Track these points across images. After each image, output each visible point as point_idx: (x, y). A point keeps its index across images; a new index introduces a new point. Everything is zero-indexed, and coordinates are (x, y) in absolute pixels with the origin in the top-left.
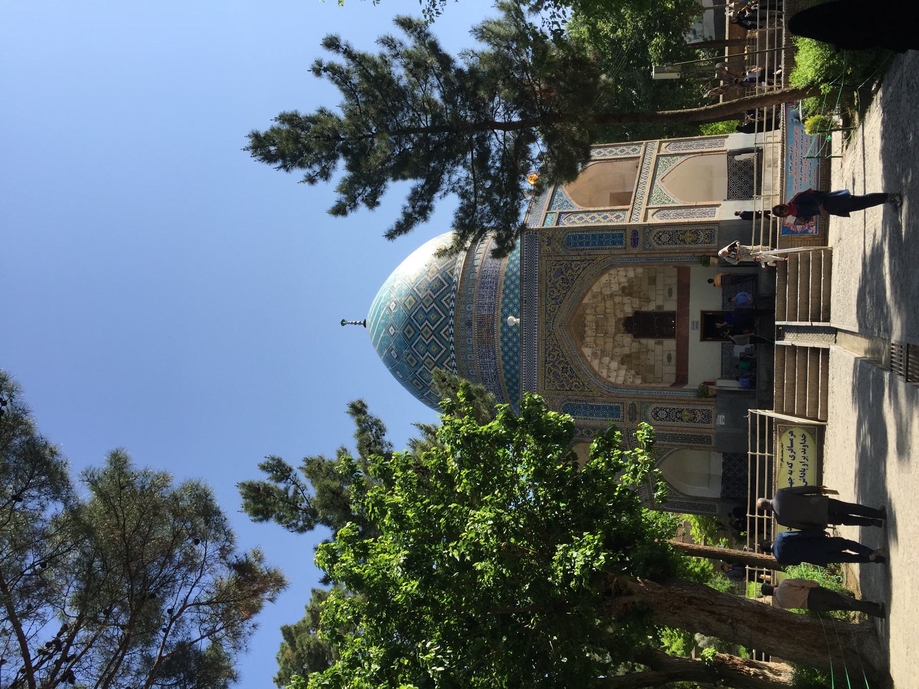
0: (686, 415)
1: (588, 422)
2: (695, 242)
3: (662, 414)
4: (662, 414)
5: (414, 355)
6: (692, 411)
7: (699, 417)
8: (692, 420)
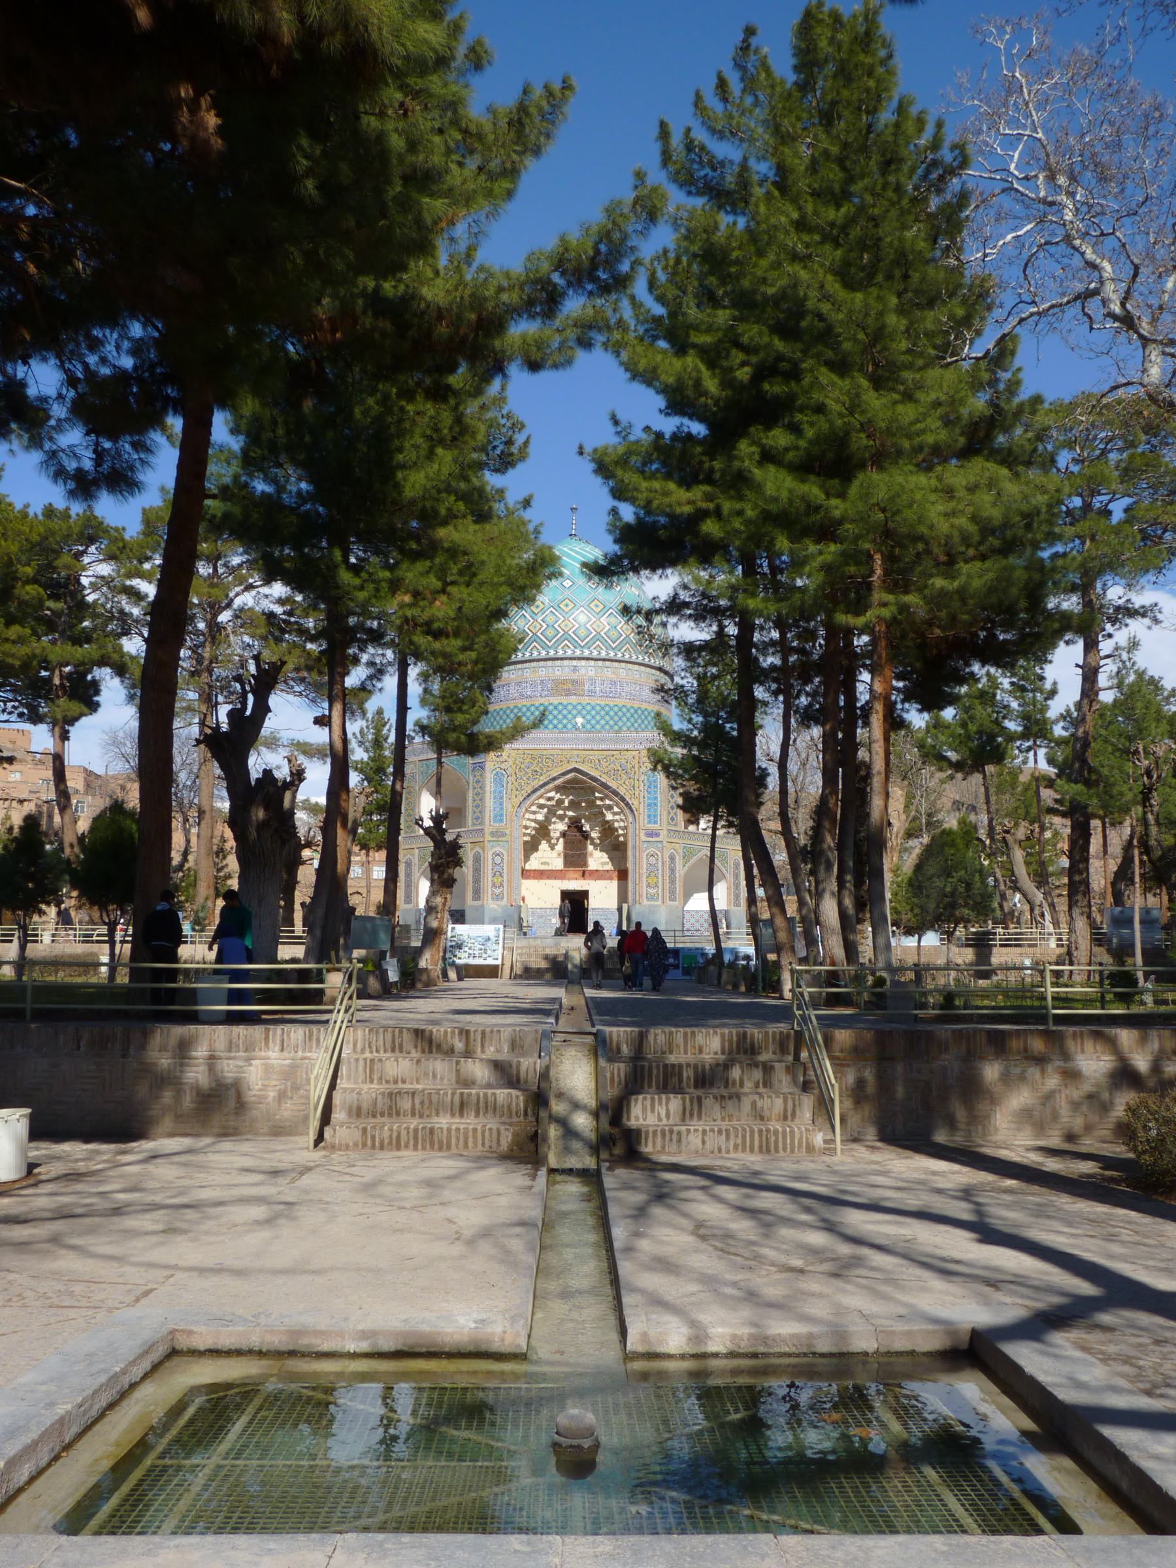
0: (498, 880)
2: (648, 886)
3: (498, 860)
4: (498, 860)
6: (502, 885)
7: (497, 891)
8: (494, 885)
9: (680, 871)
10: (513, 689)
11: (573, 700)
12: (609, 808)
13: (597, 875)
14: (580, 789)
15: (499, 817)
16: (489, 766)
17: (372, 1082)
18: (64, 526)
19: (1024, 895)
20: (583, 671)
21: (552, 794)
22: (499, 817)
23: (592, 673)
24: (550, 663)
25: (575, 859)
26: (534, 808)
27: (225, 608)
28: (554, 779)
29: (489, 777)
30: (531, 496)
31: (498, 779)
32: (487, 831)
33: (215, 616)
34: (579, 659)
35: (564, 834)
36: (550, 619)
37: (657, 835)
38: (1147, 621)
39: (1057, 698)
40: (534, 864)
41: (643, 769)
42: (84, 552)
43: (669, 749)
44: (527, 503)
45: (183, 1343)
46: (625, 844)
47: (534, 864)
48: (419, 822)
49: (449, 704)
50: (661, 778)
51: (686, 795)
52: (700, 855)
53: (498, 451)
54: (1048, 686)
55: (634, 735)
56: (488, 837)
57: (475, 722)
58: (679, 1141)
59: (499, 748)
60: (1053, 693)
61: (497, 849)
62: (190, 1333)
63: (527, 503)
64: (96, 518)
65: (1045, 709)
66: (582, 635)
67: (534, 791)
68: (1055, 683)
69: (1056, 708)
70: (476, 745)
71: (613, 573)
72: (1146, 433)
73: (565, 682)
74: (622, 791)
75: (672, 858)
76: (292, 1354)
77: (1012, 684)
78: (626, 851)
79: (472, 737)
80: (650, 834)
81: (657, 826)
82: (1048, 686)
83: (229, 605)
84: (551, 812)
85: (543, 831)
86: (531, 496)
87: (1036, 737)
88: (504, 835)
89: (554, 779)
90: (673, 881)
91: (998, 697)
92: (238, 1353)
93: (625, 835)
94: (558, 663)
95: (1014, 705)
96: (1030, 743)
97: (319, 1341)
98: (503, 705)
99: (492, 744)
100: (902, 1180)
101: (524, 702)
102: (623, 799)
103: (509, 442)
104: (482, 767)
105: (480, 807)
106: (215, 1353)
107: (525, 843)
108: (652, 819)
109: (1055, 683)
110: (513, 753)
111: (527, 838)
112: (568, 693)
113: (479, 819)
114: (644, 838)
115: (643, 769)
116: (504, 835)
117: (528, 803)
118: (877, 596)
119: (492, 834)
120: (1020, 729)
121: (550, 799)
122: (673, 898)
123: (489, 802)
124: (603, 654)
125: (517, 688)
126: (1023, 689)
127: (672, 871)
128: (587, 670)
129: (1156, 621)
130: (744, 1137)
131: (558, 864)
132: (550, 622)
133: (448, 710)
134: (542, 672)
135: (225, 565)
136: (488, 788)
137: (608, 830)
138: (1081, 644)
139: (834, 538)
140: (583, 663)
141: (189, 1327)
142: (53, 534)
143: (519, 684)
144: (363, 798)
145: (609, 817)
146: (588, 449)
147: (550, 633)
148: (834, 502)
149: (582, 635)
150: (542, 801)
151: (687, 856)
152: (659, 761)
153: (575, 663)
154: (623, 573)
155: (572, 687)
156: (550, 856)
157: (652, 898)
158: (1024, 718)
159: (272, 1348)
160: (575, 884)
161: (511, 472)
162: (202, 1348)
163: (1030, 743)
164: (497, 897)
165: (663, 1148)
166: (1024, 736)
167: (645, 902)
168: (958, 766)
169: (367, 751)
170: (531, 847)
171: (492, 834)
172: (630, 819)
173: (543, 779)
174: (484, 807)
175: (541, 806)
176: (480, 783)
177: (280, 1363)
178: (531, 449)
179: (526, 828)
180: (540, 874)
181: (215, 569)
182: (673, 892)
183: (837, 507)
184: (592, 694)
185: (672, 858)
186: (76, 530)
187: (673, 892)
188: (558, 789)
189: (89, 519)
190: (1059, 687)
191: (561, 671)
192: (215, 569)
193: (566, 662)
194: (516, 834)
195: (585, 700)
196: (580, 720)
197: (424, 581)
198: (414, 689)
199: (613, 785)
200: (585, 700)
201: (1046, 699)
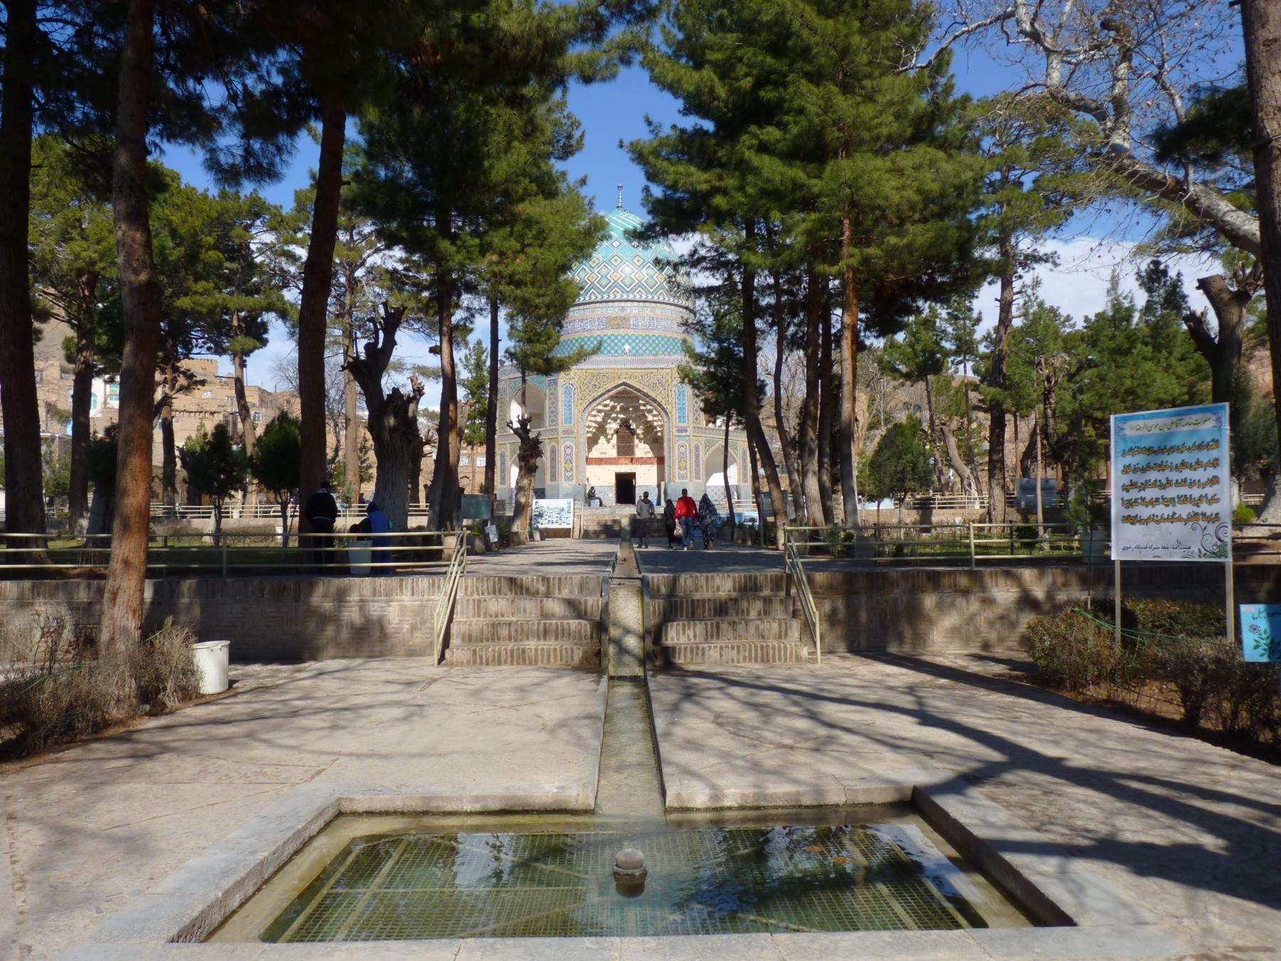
3: (568, 451)
4: (568, 451)
10: (577, 325)
11: (622, 332)
12: (650, 411)
13: (642, 461)
14: (628, 397)
15: (569, 420)
16: (561, 382)
19: (956, 470)
20: (629, 310)
21: (608, 402)
22: (569, 420)
23: (635, 311)
25: (625, 449)
30: (586, 177)
31: (568, 391)
33: (353, 272)
35: (617, 432)
36: (604, 272)
38: (1049, 265)
40: (595, 453)
42: (251, 226)
44: (583, 182)
45: (347, 807)
46: (662, 438)
47: (595, 453)
48: (509, 424)
49: (530, 337)
50: (688, 390)
51: (706, 401)
54: (975, 315)
56: (561, 435)
57: (550, 350)
60: (979, 320)
61: (568, 443)
62: (351, 800)
63: (583, 182)
65: (973, 332)
70: (550, 367)
71: (649, 237)
74: (659, 399)
75: (697, 448)
78: (662, 443)
80: (680, 430)
82: (975, 315)
84: (607, 415)
85: (601, 429)
86: (586, 177)
87: (966, 354)
90: (697, 465)
93: (662, 432)
95: (950, 330)
98: (570, 337)
99: (562, 366)
101: (586, 334)
102: (660, 405)
103: (569, 137)
105: (554, 412)
106: (370, 814)
108: (682, 419)
112: (618, 327)
113: (554, 421)
119: (564, 432)
120: (954, 348)
122: (698, 478)
123: (561, 408)
124: (644, 297)
125: (581, 324)
126: (956, 318)
127: (697, 457)
128: (632, 309)
129: (1056, 265)
131: (613, 453)
134: (599, 311)
135: (359, 233)
137: (649, 428)
142: (228, 212)
143: (581, 320)
144: (468, 407)
145: (650, 418)
146: (626, 143)
150: (600, 407)
151: (708, 445)
152: (686, 376)
155: (620, 322)
156: (607, 448)
157: (683, 477)
160: (625, 468)
164: (569, 479)
166: (957, 353)
167: (678, 481)
168: (907, 376)
170: (593, 441)
171: (564, 432)
173: (601, 391)
175: (600, 411)
176: (554, 395)
178: (586, 141)
180: (600, 461)
182: (698, 473)
184: (636, 327)
185: (697, 448)
186: (245, 208)
187: (698, 473)
188: (612, 398)
191: (613, 310)
194: (581, 432)
195: (631, 332)
196: (627, 347)
198: (503, 327)
200: (631, 332)
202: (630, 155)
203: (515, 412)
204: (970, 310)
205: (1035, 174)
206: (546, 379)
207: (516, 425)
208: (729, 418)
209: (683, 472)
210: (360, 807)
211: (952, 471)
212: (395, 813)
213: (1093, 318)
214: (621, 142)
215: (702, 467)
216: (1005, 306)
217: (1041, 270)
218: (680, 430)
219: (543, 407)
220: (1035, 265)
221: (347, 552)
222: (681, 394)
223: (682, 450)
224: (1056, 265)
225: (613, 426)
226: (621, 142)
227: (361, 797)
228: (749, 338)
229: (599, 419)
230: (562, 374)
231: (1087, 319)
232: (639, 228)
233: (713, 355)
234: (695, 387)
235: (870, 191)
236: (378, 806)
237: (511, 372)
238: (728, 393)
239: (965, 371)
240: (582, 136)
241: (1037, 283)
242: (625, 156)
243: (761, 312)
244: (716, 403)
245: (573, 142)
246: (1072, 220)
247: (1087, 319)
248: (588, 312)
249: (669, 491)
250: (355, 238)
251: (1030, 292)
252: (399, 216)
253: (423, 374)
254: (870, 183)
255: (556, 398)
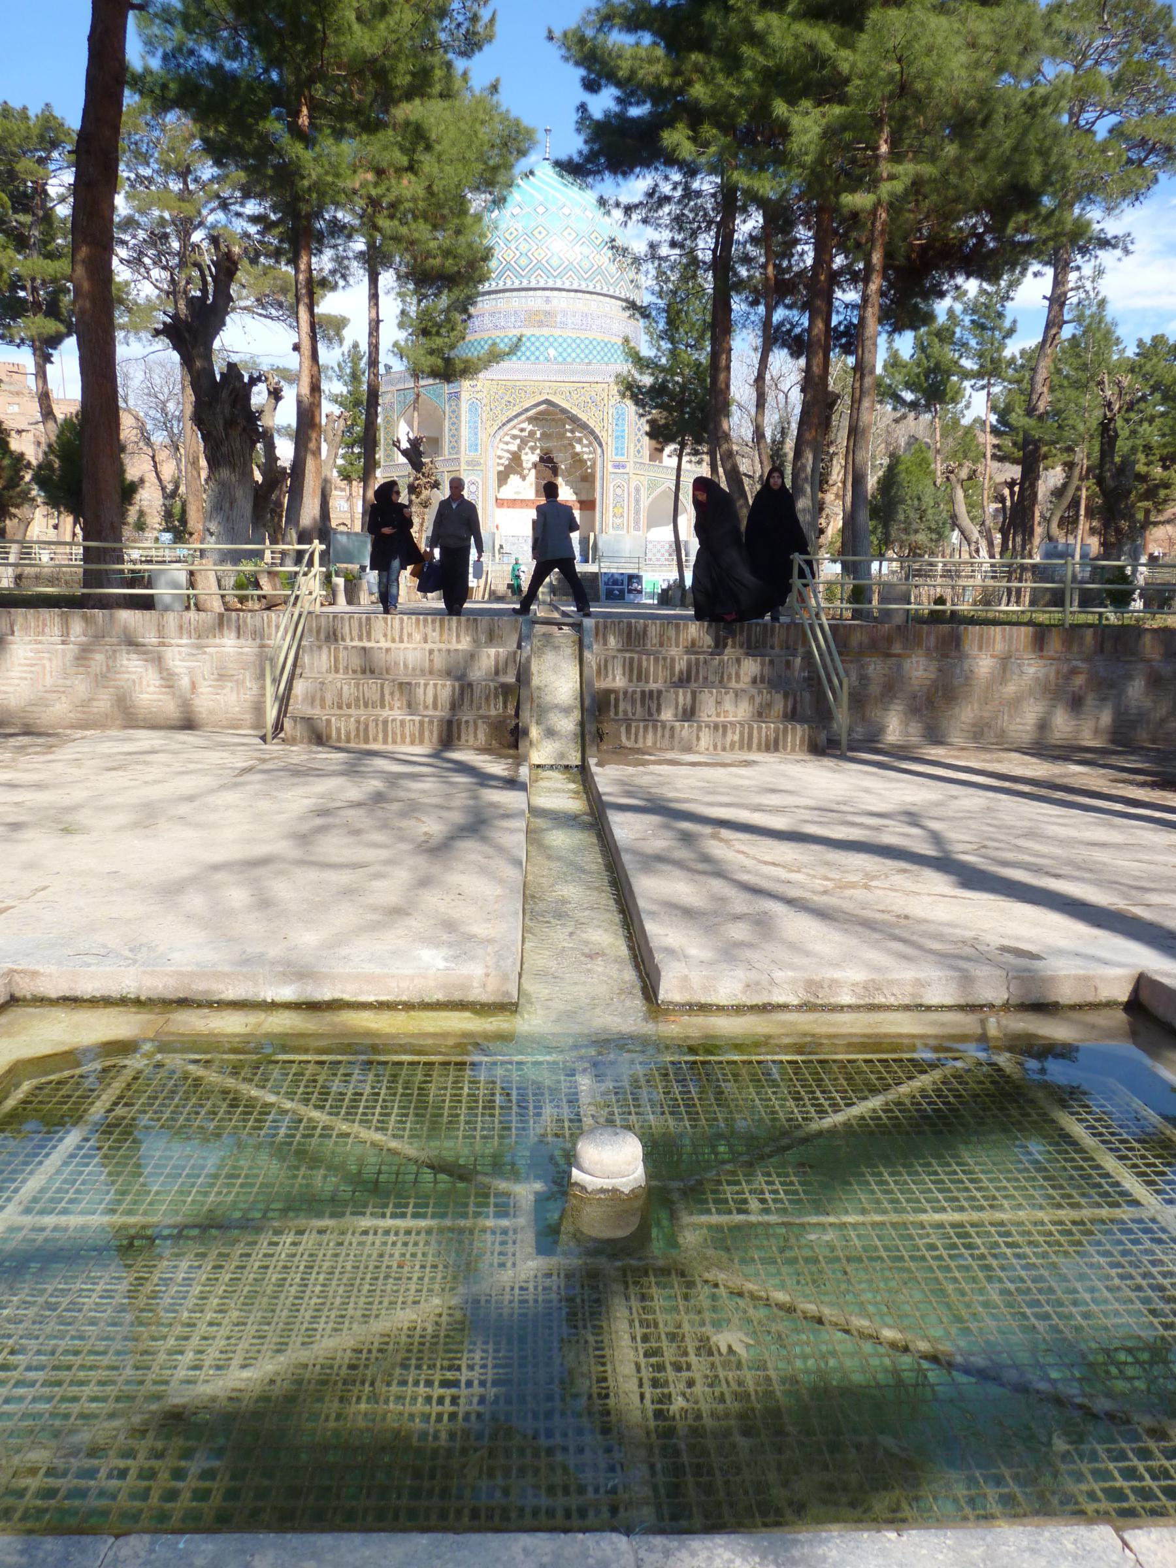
1: (463, 424)
5: (517, 238)
9: (645, 502)
10: (486, 319)
11: (546, 331)
12: (579, 441)
14: (552, 420)
15: (474, 447)
16: (464, 396)
17: (337, 671)
18: (23, 127)
19: (963, 533)
20: (555, 302)
21: (525, 425)
22: (474, 447)
23: (563, 305)
24: (523, 293)
26: (507, 439)
27: (196, 228)
28: (527, 410)
29: (464, 406)
30: (497, 80)
31: (473, 409)
32: (463, 461)
33: (188, 235)
34: (552, 289)
35: (535, 465)
36: (524, 247)
37: (624, 467)
38: (1118, 252)
39: (1015, 336)
40: (507, 492)
41: (612, 402)
42: (48, 158)
43: (637, 376)
44: (494, 88)
45: (25, 988)
46: (593, 475)
47: (507, 492)
48: (396, 444)
49: (426, 328)
50: (630, 408)
51: (652, 423)
52: (663, 487)
53: (463, 30)
54: (1007, 324)
55: (604, 367)
57: (452, 347)
58: (672, 736)
59: (477, 371)
60: (1010, 332)
62: (35, 974)
63: (494, 88)
64: (55, 118)
65: (1002, 346)
66: (555, 265)
67: (509, 421)
68: (1015, 322)
69: (1012, 349)
70: (449, 371)
71: (589, 173)
72: (1144, 41)
73: (537, 313)
74: (591, 424)
75: (637, 490)
76: (184, 1003)
77: (973, 321)
78: (593, 482)
79: (448, 361)
80: (617, 466)
81: (624, 458)
82: (1007, 324)
83: (201, 224)
84: (524, 442)
85: (516, 460)
86: (497, 80)
87: (991, 375)
88: (479, 464)
89: (527, 410)
90: (637, 512)
91: (958, 335)
92: (107, 1002)
93: (594, 464)
94: (531, 293)
95: (973, 343)
96: (985, 382)
97: (221, 987)
98: (478, 336)
99: (468, 370)
100: (146, 763)
101: (498, 333)
102: (592, 432)
103: (475, 19)
104: (456, 396)
105: (456, 437)
106: (72, 1002)
107: (499, 473)
108: (619, 451)
109: (1015, 322)
110: (488, 383)
111: (502, 468)
112: (541, 324)
113: (455, 448)
114: (611, 469)
115: (612, 402)
116: (479, 464)
117: (501, 433)
118: (885, 168)
119: (468, 463)
120: (976, 367)
121: (522, 430)
122: (637, 529)
123: (465, 431)
125: (493, 317)
126: (983, 327)
127: (637, 501)
128: (560, 301)
129: (1127, 252)
130: (742, 733)
132: (524, 251)
133: (425, 332)
134: (515, 302)
135: (196, 180)
136: (463, 418)
137: (578, 460)
138: (1049, 272)
139: (842, 100)
140: (556, 293)
141: (32, 967)
142: (11, 135)
143: (492, 314)
144: (342, 421)
145: (578, 448)
146: (557, 34)
147: (523, 261)
148: (845, 53)
149: (555, 265)
150: (515, 432)
151: (651, 487)
152: (631, 390)
153: (547, 293)
154: (599, 172)
155: (543, 318)
157: (618, 527)
158: (980, 357)
159: (153, 995)
161: (478, 57)
162: (53, 995)
163: (985, 382)
165: (655, 743)
166: (979, 375)
167: (611, 531)
168: (913, 405)
169: (346, 384)
170: (503, 478)
171: (468, 463)
172: (599, 451)
174: (459, 437)
175: (514, 437)
176: (456, 413)
177: (161, 1019)
178: (498, 27)
179: (500, 458)
180: (513, 503)
181: (185, 183)
182: (637, 522)
183: (845, 60)
184: (564, 325)
185: (637, 490)
186: (35, 132)
187: (637, 522)
188: (531, 420)
189: (47, 120)
190: (1019, 326)
191: (534, 301)
192: (185, 183)
193: (539, 293)
194: (490, 463)
195: (557, 332)
196: (552, 352)
197: (387, 156)
198: (390, 307)
199: (583, 417)
200: (557, 332)
201: (1004, 338)
202: (563, 52)
203: (404, 433)
204: (1000, 315)
205: (1113, 119)
206: (447, 388)
207: (405, 445)
208: (683, 445)
209: (618, 521)
210: (53, 990)
211: (956, 533)
212: (122, 1002)
213: (1148, 341)
214: (550, 32)
215: (643, 515)
216: (1057, 300)
217: (1106, 257)
218: (616, 466)
219: (441, 430)
220: (1099, 253)
221: (152, 596)
222: (620, 417)
223: (619, 491)
224: (1127, 252)
225: (530, 458)
226: (550, 32)
227: (52, 969)
228: (720, 327)
229: (514, 447)
230: (466, 384)
231: (1141, 343)
232: (576, 159)
233: (664, 361)
234: (638, 402)
235: (928, 63)
236: (87, 988)
237: (400, 380)
238: (683, 413)
239: (975, 405)
240: (492, 20)
241: (1099, 272)
242: (554, 52)
243: (740, 285)
244: (666, 426)
245: (480, 27)
246: (1155, 188)
247: (1141, 343)
248: (502, 303)
249: (600, 545)
250: (192, 187)
251: (1088, 285)
252: (229, 117)
253: (284, 378)
254: (929, 50)
255: (458, 417)
